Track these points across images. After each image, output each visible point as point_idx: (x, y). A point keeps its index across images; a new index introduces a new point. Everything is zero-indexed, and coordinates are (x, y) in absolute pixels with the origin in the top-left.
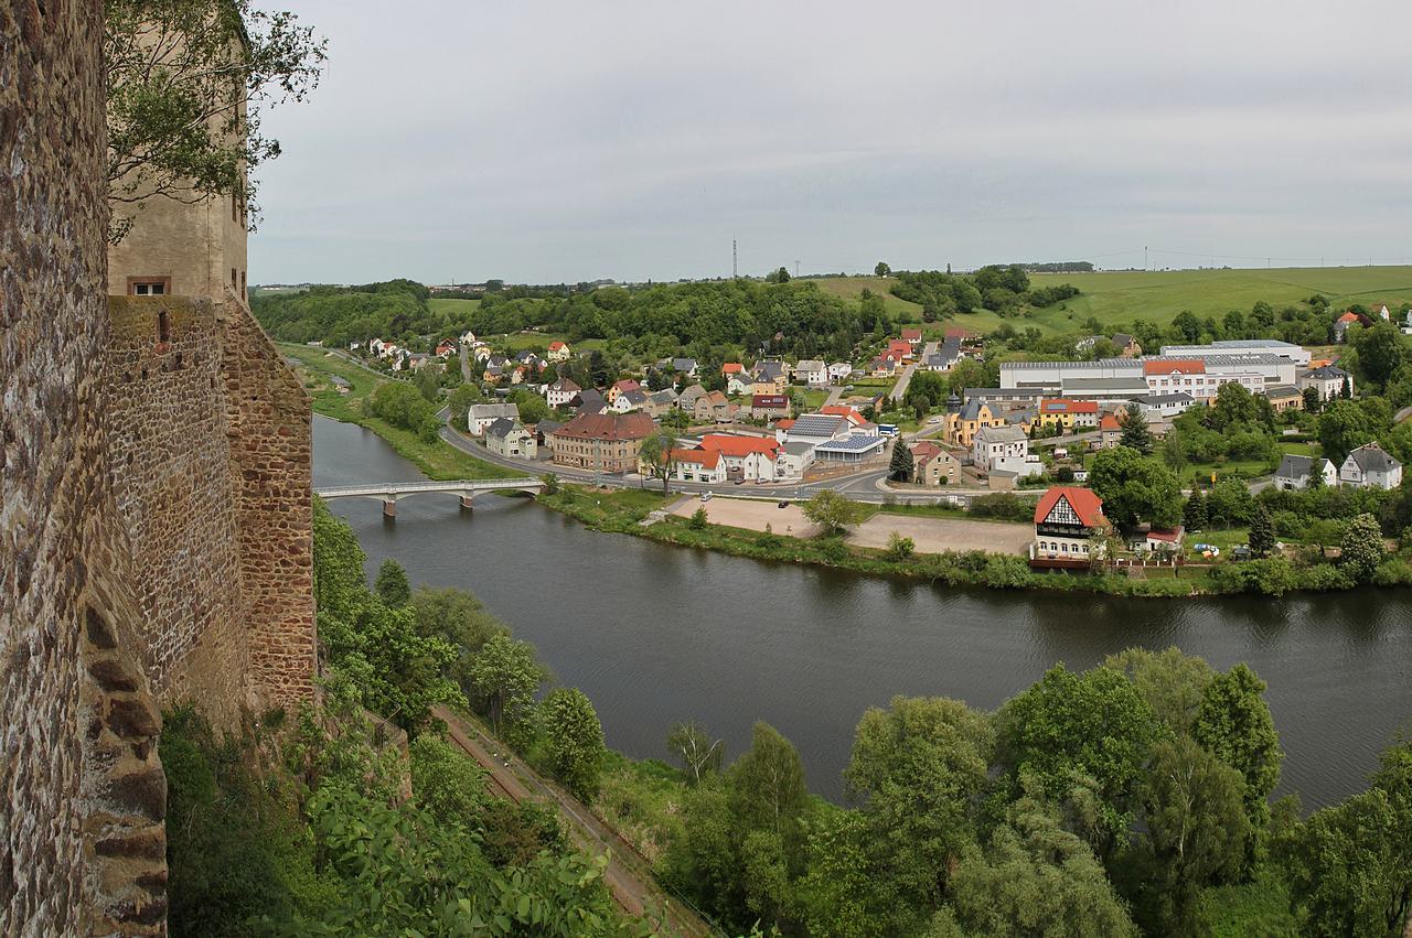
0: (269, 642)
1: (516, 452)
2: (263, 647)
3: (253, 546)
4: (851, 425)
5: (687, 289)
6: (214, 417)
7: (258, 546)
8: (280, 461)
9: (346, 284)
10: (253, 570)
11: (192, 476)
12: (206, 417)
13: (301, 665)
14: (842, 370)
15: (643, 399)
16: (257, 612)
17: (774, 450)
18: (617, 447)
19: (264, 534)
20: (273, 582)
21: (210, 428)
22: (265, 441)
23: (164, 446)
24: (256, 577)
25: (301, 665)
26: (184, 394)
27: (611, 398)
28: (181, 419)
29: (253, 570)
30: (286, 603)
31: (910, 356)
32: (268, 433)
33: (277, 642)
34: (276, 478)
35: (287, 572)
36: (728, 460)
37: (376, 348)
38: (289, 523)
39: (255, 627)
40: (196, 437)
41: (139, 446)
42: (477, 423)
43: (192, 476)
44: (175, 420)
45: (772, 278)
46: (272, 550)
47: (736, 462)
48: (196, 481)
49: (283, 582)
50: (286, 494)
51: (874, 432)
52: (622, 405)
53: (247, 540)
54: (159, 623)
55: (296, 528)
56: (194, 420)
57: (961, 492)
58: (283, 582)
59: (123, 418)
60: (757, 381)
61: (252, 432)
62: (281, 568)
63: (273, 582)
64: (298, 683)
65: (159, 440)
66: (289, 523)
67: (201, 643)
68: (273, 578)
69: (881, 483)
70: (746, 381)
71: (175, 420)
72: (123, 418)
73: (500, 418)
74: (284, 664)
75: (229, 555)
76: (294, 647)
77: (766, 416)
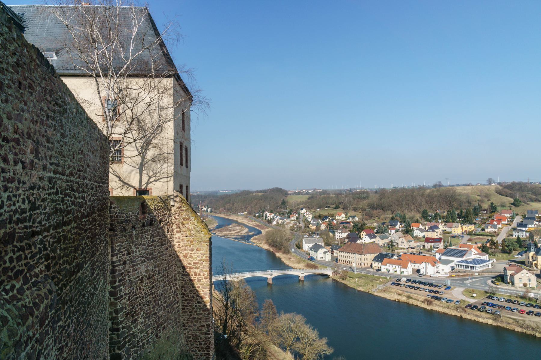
0: (193, 335)
1: (322, 258)
2: (190, 337)
3: (186, 296)
4: (473, 253)
5: (395, 191)
6: (169, 244)
7: (188, 296)
8: (197, 261)
9: (255, 190)
10: (186, 306)
11: (157, 269)
12: (165, 244)
13: (206, 344)
14: (470, 228)
15: (375, 237)
16: (187, 323)
17: (435, 262)
18: (363, 257)
19: (191, 291)
20: (194, 310)
21: (167, 249)
22: (191, 254)
23: (143, 257)
24: (187, 309)
25: (206, 344)
26: (153, 236)
27: (361, 236)
28: (152, 246)
29: (186, 306)
30: (200, 319)
31: (506, 222)
32: (192, 250)
33: (196, 335)
34: (195, 268)
35: (200, 306)
36: (413, 265)
37: (266, 215)
38: (201, 286)
39: (187, 329)
40: (159, 253)
41: (129, 257)
42: (306, 246)
43: (157, 269)
44: (148, 246)
45: (435, 186)
46: (194, 297)
47: (417, 267)
48: (159, 271)
49: (198, 310)
50: (199, 274)
51: (486, 257)
52: (366, 239)
53: (184, 294)
54: (138, 330)
55: (204, 288)
56: (158, 246)
57: (536, 292)
58: (198, 310)
59: (122, 246)
60: (427, 231)
61: (185, 250)
62: (198, 305)
63: (194, 310)
64: (204, 351)
65: (140, 254)
66: (201, 286)
67: (160, 337)
68: (194, 308)
69: (489, 282)
70: (422, 231)
71: (148, 246)
72: (122, 246)
73: (316, 244)
74: (199, 344)
75: (175, 300)
76: (202, 336)
77: (431, 246)
